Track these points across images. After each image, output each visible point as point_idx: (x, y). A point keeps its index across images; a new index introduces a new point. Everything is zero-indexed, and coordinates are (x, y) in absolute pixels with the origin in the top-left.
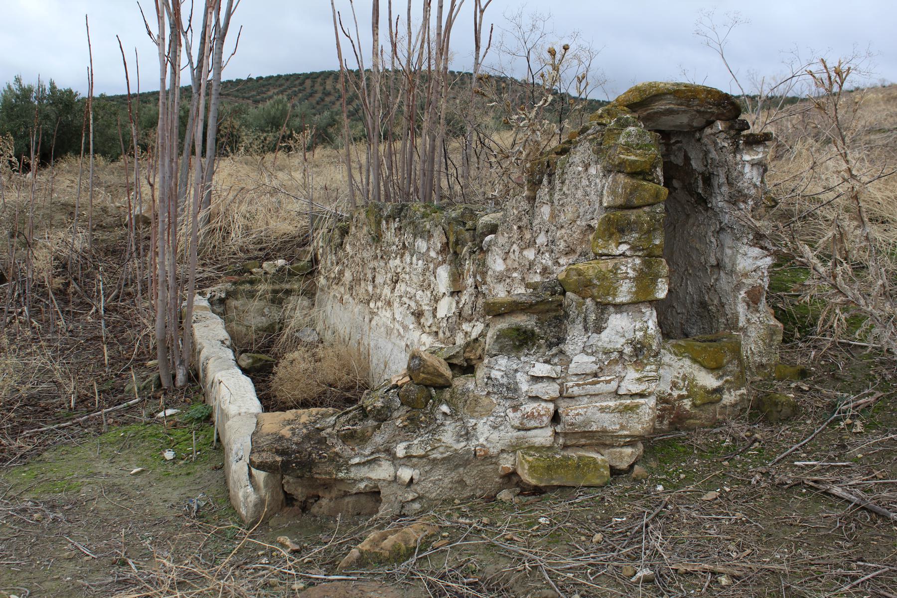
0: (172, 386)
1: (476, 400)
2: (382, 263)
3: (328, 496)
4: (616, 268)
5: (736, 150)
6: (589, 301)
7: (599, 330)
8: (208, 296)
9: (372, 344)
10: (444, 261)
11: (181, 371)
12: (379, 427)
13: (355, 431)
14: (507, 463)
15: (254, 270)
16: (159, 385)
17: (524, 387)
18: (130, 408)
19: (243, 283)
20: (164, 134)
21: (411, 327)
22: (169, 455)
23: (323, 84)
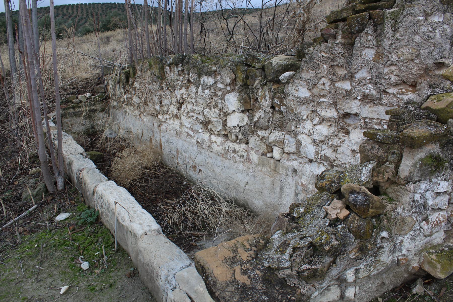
0: (56, 190)
2: (168, 92)
8: (52, 119)
9: (163, 140)
10: (233, 90)
11: (60, 179)
12: (334, 262)
13: (316, 270)
15: (74, 101)
16: (47, 191)
18: (31, 214)
19: (69, 108)
21: (200, 131)
22: (85, 265)
23: (62, 11)
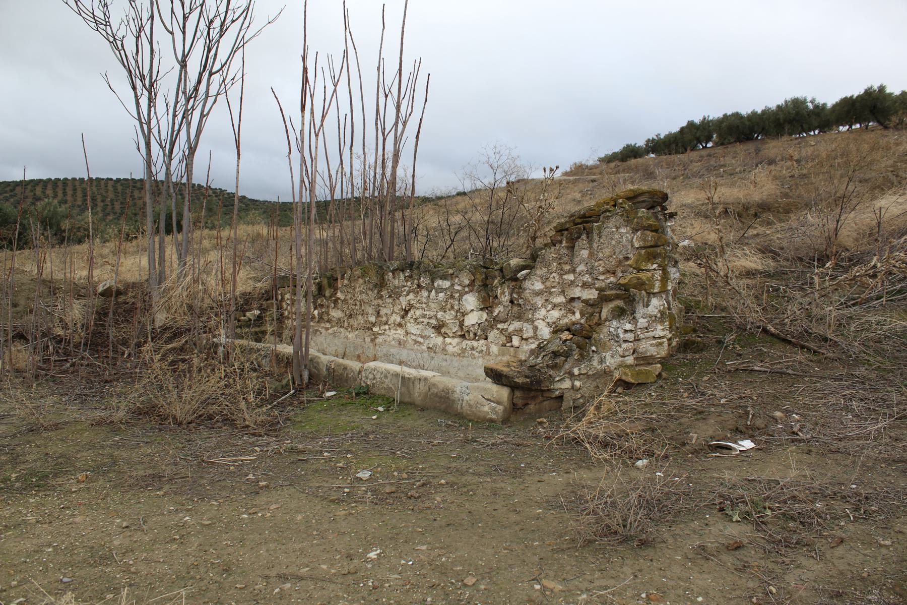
1: (605, 343)
3: (534, 403)
4: (653, 275)
5: (666, 221)
6: (643, 292)
7: (648, 306)
14: (617, 375)
17: (621, 336)
20: (297, 215)
